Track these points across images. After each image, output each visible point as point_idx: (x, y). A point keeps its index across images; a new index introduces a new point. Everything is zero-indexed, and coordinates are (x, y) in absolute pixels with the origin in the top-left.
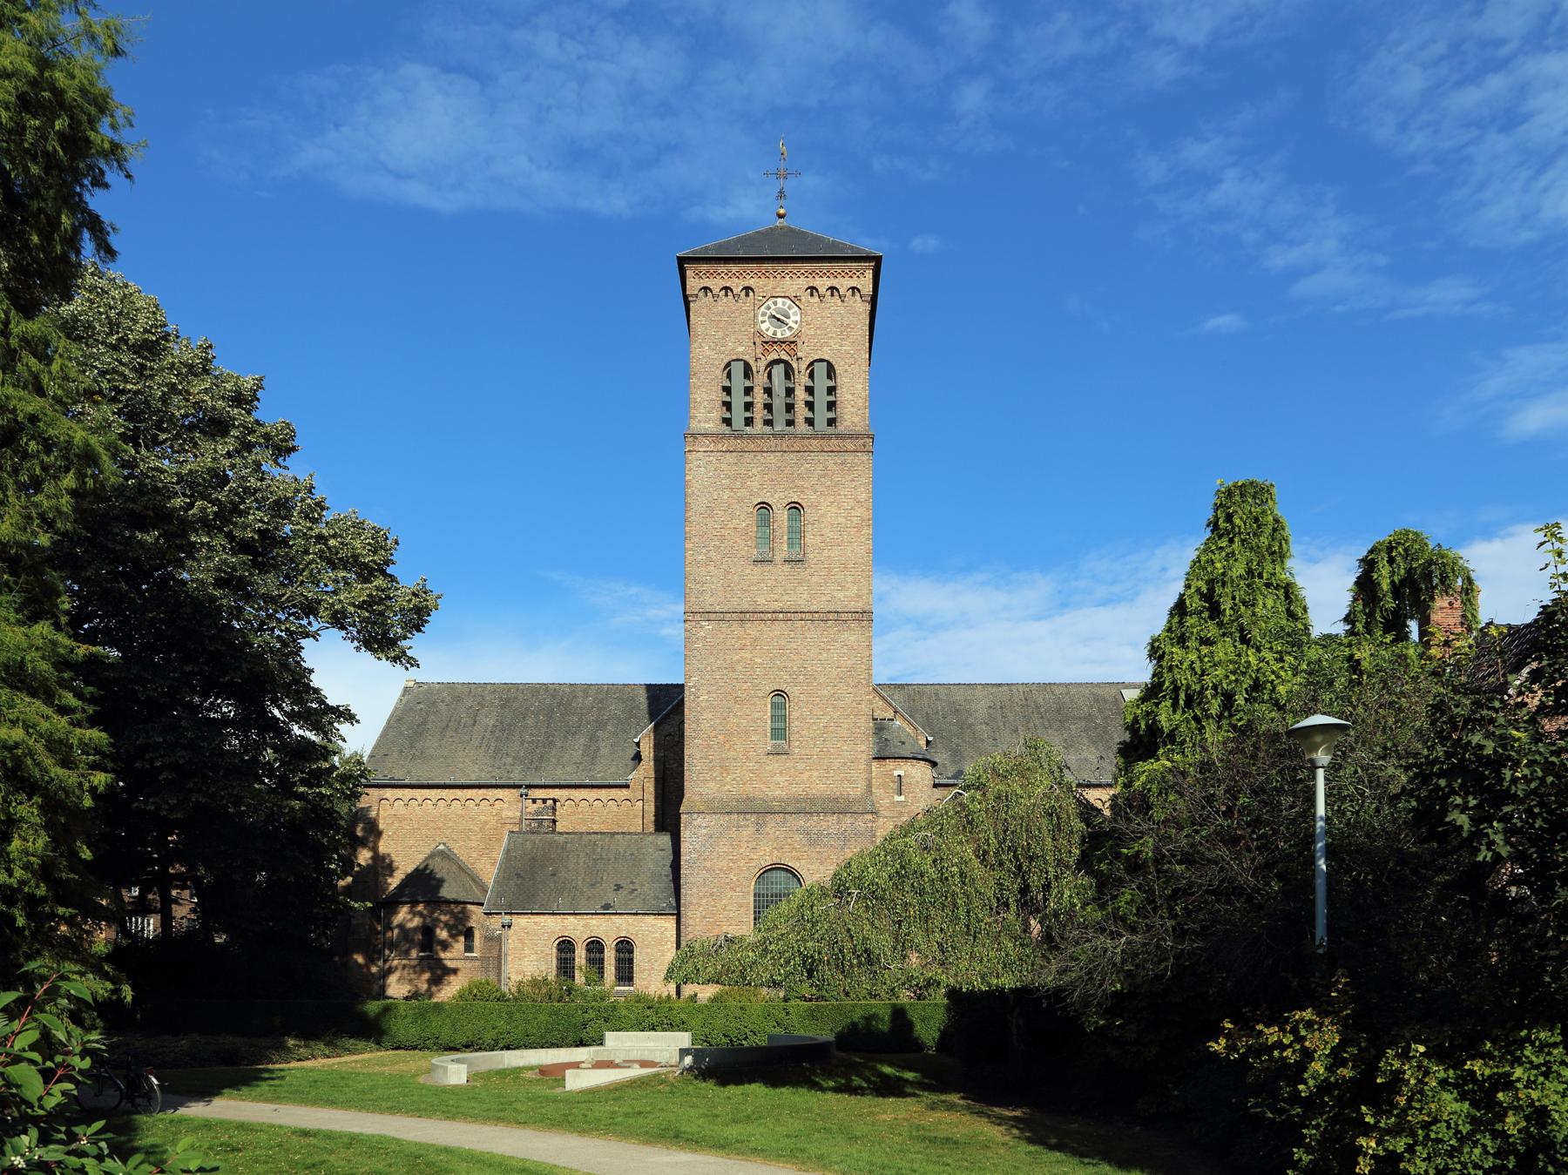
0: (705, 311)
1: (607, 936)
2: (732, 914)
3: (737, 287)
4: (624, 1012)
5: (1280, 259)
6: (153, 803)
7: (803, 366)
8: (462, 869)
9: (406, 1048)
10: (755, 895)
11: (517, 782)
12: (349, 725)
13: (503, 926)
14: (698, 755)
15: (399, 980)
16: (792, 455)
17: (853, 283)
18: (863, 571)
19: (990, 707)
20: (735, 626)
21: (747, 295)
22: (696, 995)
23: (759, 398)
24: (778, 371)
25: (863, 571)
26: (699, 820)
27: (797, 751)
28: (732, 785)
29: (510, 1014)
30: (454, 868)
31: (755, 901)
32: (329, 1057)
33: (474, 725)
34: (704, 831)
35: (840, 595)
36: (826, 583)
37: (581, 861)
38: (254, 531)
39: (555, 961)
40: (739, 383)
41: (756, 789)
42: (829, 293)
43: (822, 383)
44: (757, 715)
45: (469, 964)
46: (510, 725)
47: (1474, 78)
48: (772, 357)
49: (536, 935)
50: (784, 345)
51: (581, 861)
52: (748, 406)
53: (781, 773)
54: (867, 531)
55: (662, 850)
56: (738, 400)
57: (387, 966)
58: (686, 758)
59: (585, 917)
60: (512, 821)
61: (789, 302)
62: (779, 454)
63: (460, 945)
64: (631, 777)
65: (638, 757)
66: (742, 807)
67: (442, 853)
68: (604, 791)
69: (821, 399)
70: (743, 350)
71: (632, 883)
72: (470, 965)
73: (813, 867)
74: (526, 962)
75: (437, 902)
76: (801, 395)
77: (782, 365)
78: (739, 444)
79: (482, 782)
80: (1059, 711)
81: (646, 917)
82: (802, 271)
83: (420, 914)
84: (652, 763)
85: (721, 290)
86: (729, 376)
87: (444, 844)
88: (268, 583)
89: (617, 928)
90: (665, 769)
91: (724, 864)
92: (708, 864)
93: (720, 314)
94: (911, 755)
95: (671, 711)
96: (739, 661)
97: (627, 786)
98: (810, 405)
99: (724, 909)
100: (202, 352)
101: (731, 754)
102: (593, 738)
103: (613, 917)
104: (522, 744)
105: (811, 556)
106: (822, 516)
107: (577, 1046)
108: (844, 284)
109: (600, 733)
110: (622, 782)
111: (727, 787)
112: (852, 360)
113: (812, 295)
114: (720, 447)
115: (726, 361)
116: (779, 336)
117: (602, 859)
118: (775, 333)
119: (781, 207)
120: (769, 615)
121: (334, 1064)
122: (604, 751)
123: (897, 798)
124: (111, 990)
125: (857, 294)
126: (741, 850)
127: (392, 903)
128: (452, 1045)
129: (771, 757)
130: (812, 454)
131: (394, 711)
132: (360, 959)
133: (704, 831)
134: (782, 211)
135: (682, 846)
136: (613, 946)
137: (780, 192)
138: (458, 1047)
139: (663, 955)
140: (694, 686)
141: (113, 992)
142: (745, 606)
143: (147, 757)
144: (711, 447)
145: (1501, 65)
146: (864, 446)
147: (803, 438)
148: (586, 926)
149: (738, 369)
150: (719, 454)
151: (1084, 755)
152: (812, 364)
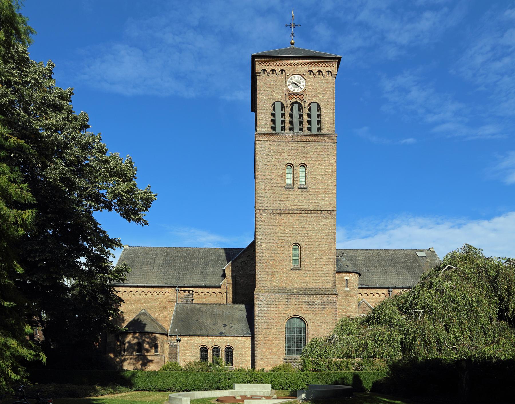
0: (263, 80)
1: (222, 346)
2: (276, 336)
3: (278, 70)
4: (237, 376)
5: (431, 119)
6: (35, 277)
7: (307, 105)
8: (152, 320)
9: (141, 390)
10: (286, 328)
11: (174, 285)
12: (119, 248)
13: (177, 341)
14: (262, 270)
15: (129, 364)
16: (302, 143)
19: (364, 258)
20: (278, 216)
21: (282, 73)
23: (287, 118)
24: (296, 107)
25: (332, 193)
26: (262, 297)
28: (276, 282)
29: (187, 377)
30: (149, 319)
31: (286, 331)
32: (114, 394)
33: (154, 263)
34: (264, 302)
35: (322, 203)
36: (316, 198)
38: (75, 156)
39: (199, 355)
40: (278, 112)
41: (286, 284)
42: (318, 73)
43: (314, 113)
44: (287, 253)
45: (156, 358)
46: (169, 263)
47: (499, 59)
48: (294, 100)
50: (298, 96)
51: (208, 315)
52: (283, 122)
53: (297, 278)
56: (278, 119)
57: (123, 358)
58: (256, 271)
59: (212, 337)
60: (172, 301)
61: (301, 77)
62: (296, 143)
63: (153, 351)
64: (221, 283)
65: (224, 276)
66: (281, 292)
67: (144, 313)
68: (210, 289)
69: (314, 119)
70: (281, 97)
71: (231, 324)
72: (157, 358)
73: (311, 317)
74: (187, 356)
75: (143, 333)
76: (305, 117)
77: (297, 104)
78: (279, 138)
79: (160, 285)
80: (392, 260)
81: (238, 337)
82: (306, 63)
83: (137, 338)
84: (231, 278)
85: (271, 71)
86: (274, 109)
87: (144, 310)
88: (81, 182)
90: (236, 280)
91: (273, 315)
92: (266, 315)
93: (270, 81)
94: (352, 271)
96: (279, 231)
97: (220, 287)
98: (309, 122)
99: (273, 334)
100: (49, 67)
101: (275, 270)
102: (204, 268)
103: (224, 337)
104: (175, 270)
105: (310, 186)
106: (315, 169)
107: (216, 390)
108: (324, 69)
109: (207, 267)
110: (218, 285)
112: (328, 103)
113: (310, 74)
114: (270, 139)
115: (273, 102)
116: (296, 91)
117: (216, 314)
118: (294, 90)
119: (292, 40)
120: (292, 211)
121: (118, 397)
122: (209, 273)
123: (346, 289)
124: (34, 355)
125: (330, 74)
126: (280, 310)
127: (125, 334)
128: (162, 389)
129: (293, 271)
130: (311, 143)
131: (121, 257)
132: (112, 356)
133: (264, 302)
134: (293, 41)
135: (255, 307)
136: (224, 349)
137: (292, 33)
139: (245, 353)
140: (260, 241)
141: (36, 356)
142: (282, 207)
143: (32, 256)
144: (267, 139)
146: (333, 140)
148: (212, 341)
149: (278, 106)
150: (270, 142)
151: (405, 276)
152: (310, 104)
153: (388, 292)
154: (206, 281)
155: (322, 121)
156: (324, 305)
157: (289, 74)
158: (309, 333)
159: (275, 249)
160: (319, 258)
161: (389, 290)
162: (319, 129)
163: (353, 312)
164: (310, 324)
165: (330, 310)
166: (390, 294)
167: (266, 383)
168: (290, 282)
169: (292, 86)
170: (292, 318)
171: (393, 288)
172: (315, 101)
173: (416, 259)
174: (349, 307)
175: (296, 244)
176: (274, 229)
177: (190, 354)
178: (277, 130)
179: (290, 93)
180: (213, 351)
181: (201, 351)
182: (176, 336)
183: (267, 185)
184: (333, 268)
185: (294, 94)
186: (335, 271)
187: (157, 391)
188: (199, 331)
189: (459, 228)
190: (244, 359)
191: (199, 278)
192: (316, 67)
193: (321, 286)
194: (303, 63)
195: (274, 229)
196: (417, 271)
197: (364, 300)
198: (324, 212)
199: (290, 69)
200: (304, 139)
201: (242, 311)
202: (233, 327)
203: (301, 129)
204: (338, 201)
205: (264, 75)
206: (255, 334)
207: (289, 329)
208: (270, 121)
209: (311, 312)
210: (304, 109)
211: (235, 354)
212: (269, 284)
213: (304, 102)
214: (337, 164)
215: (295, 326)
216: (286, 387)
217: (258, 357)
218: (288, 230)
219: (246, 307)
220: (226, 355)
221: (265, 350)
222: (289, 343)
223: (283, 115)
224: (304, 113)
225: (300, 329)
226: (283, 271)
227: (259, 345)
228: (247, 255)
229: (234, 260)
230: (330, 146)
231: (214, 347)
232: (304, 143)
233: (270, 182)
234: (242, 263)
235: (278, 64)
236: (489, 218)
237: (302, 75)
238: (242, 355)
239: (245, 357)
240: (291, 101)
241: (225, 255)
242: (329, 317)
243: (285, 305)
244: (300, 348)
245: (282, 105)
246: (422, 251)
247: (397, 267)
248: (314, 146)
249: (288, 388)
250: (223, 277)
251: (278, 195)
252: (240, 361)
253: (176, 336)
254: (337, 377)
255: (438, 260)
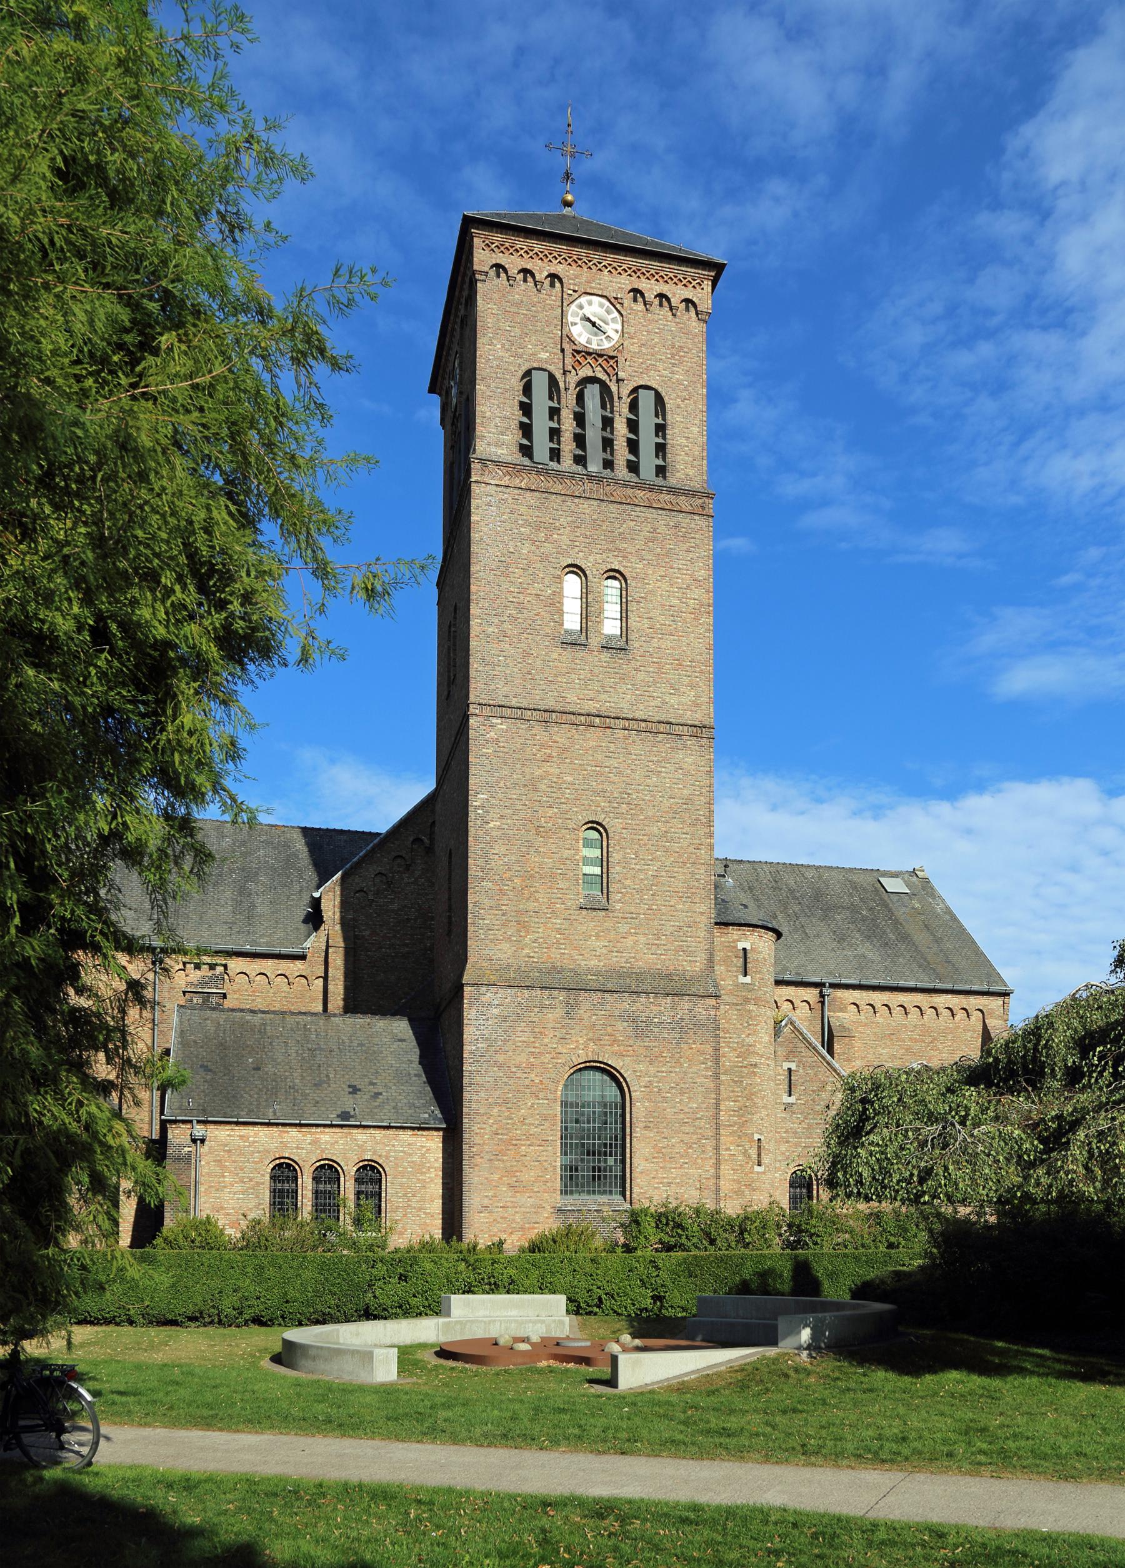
1: (347, 1160)
2: (533, 1130)
3: (541, 271)
5: (792, 488)
7: (625, 391)
16: (612, 507)
17: (688, 293)
18: (701, 672)
20: (538, 728)
21: (552, 285)
22: (501, 1243)
24: (592, 393)
26: (488, 996)
27: (618, 906)
34: (496, 1011)
35: (673, 701)
37: (292, 1051)
41: (565, 956)
44: (566, 853)
47: (967, 342)
48: (586, 372)
49: (240, 1154)
50: (600, 360)
51: (292, 1051)
52: (555, 433)
53: (597, 936)
54: (707, 620)
55: (400, 1040)
56: (541, 424)
58: (470, 906)
59: (314, 1130)
61: (608, 304)
62: (595, 503)
64: (307, 944)
65: (315, 919)
66: (547, 981)
68: (270, 963)
69: (648, 439)
70: (547, 357)
71: (372, 1084)
73: (641, 1067)
74: (226, 1195)
76: (621, 428)
77: (597, 386)
78: (543, 482)
81: (401, 1132)
82: (624, 266)
84: (338, 927)
85: (519, 272)
89: (360, 1147)
91: (523, 1058)
92: (500, 1058)
93: (519, 304)
94: (760, 923)
95: (365, 856)
96: (542, 778)
97: (303, 957)
101: (531, 905)
102: (242, 891)
103: (355, 1131)
105: (636, 645)
108: (677, 293)
109: (251, 885)
110: (296, 951)
111: (526, 951)
113: (635, 300)
114: (516, 482)
115: (524, 368)
116: (594, 346)
120: (583, 718)
122: (262, 908)
123: (742, 979)
125: (692, 309)
128: (170, 1317)
129: (584, 912)
130: (637, 509)
133: (496, 1011)
134: (569, 197)
138: (179, 1319)
140: (482, 807)
142: (551, 704)
144: (506, 481)
145: (990, 334)
146: (703, 508)
147: (626, 486)
148: (315, 1142)
149: (540, 384)
150: (516, 491)
151: (861, 950)
152: (635, 390)
153: (818, 999)
154: (254, 933)
155: (669, 446)
156: (681, 1028)
157: (575, 291)
158: (634, 1120)
159: (531, 838)
160: (663, 873)
161: (821, 992)
162: (661, 471)
163: (762, 1056)
164: (637, 1092)
165: (697, 1047)
166: (823, 1003)
167: (525, 1292)
168: (575, 949)
169: (584, 326)
170: (580, 1070)
171: (832, 986)
172: (649, 384)
173: (882, 899)
174: (750, 1040)
175: (595, 825)
176: (527, 770)
177: (238, 1187)
178: (537, 457)
179: (575, 347)
180: (314, 1179)
181: (273, 1178)
182: (191, 1122)
183: (506, 626)
184: (704, 910)
185: (590, 354)
186: (713, 921)
187: (151, 1322)
188: (268, 1106)
189: (876, 818)
190: (420, 1209)
191: (230, 925)
192: (653, 281)
193: (672, 968)
194: (615, 265)
195: (527, 770)
196: (891, 935)
197: (794, 1018)
198: (677, 727)
199: (576, 277)
200: (619, 493)
201: (404, 1040)
202: (381, 1094)
203: (608, 464)
204: (720, 699)
205: (496, 281)
206: (465, 1120)
207: (571, 1107)
208: (515, 425)
209: (641, 1051)
210: (616, 404)
211: (391, 1189)
212: (510, 952)
213: (618, 381)
214: (714, 583)
215: (589, 1096)
216: (588, 1305)
217: (473, 1200)
218: (569, 779)
219: (413, 1028)
220: (316, 1193)
221: (496, 1177)
222: (571, 1153)
223: (554, 413)
224: (617, 415)
225: (605, 1106)
226: (553, 912)
227: (478, 1160)
228: (394, 854)
229: (351, 868)
230: (693, 526)
231: (318, 1164)
232: (619, 506)
233: (516, 619)
234: (377, 880)
235: (541, 255)
236: (952, 793)
237: (613, 300)
238: (414, 1195)
239: (423, 1200)
240: (580, 373)
241: (306, 849)
242: (694, 1069)
243: (559, 1026)
244: (605, 1171)
245: (553, 381)
246: (895, 875)
247: (835, 920)
248: (646, 519)
249: (596, 1309)
250: (310, 925)
251: (539, 663)
252: (405, 1215)
253: (191, 1122)
254: (747, 1272)
255: (942, 906)
